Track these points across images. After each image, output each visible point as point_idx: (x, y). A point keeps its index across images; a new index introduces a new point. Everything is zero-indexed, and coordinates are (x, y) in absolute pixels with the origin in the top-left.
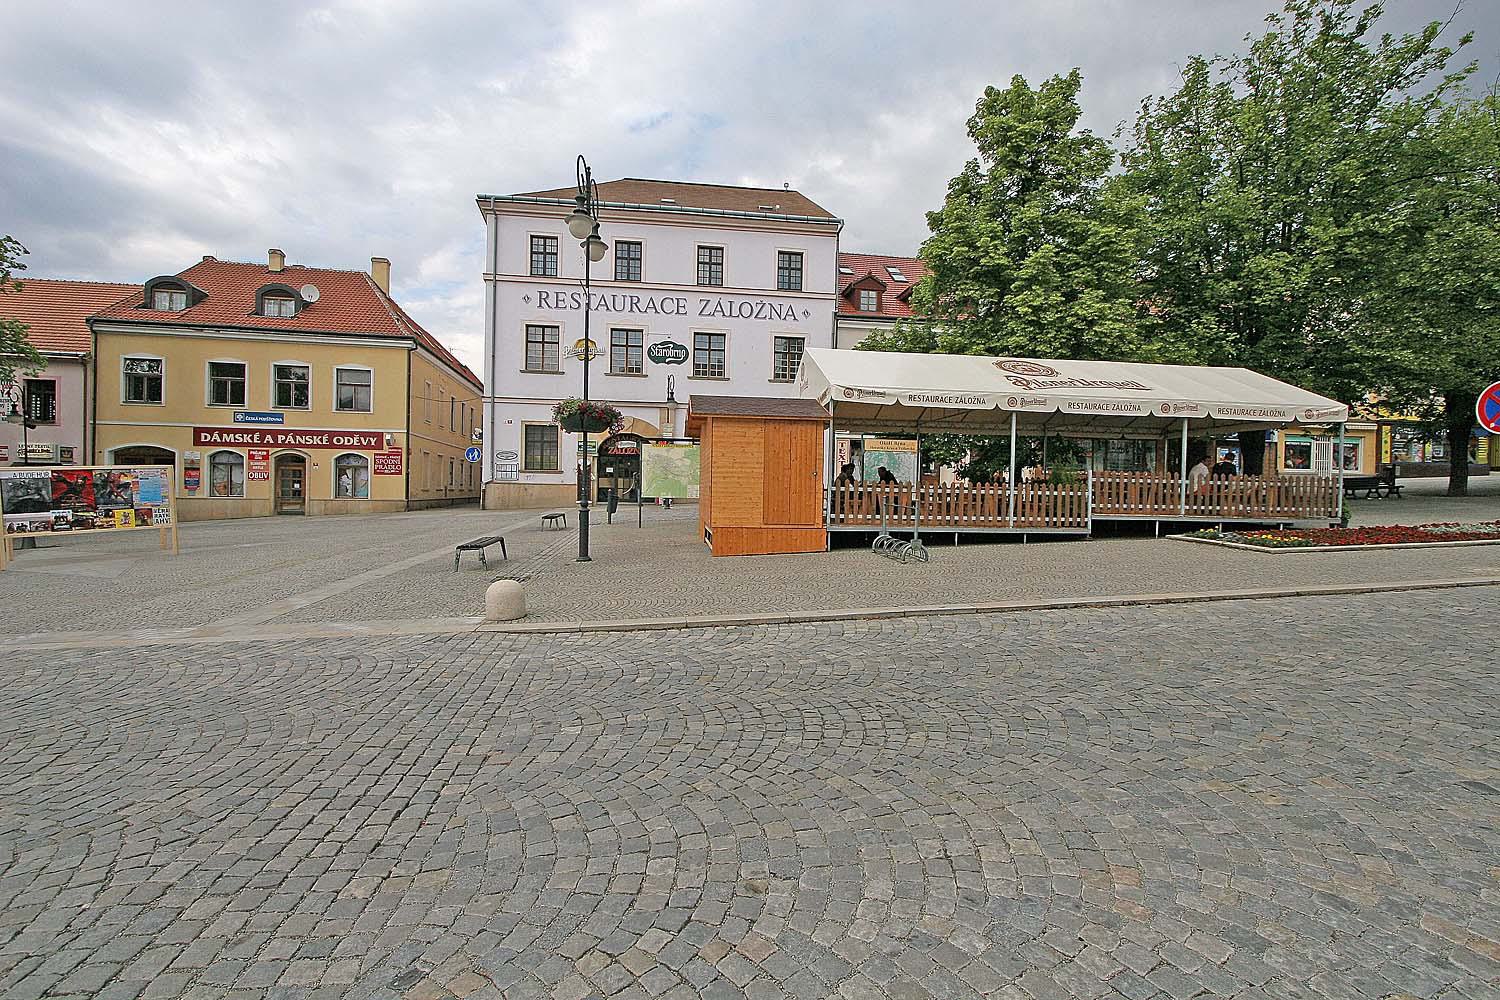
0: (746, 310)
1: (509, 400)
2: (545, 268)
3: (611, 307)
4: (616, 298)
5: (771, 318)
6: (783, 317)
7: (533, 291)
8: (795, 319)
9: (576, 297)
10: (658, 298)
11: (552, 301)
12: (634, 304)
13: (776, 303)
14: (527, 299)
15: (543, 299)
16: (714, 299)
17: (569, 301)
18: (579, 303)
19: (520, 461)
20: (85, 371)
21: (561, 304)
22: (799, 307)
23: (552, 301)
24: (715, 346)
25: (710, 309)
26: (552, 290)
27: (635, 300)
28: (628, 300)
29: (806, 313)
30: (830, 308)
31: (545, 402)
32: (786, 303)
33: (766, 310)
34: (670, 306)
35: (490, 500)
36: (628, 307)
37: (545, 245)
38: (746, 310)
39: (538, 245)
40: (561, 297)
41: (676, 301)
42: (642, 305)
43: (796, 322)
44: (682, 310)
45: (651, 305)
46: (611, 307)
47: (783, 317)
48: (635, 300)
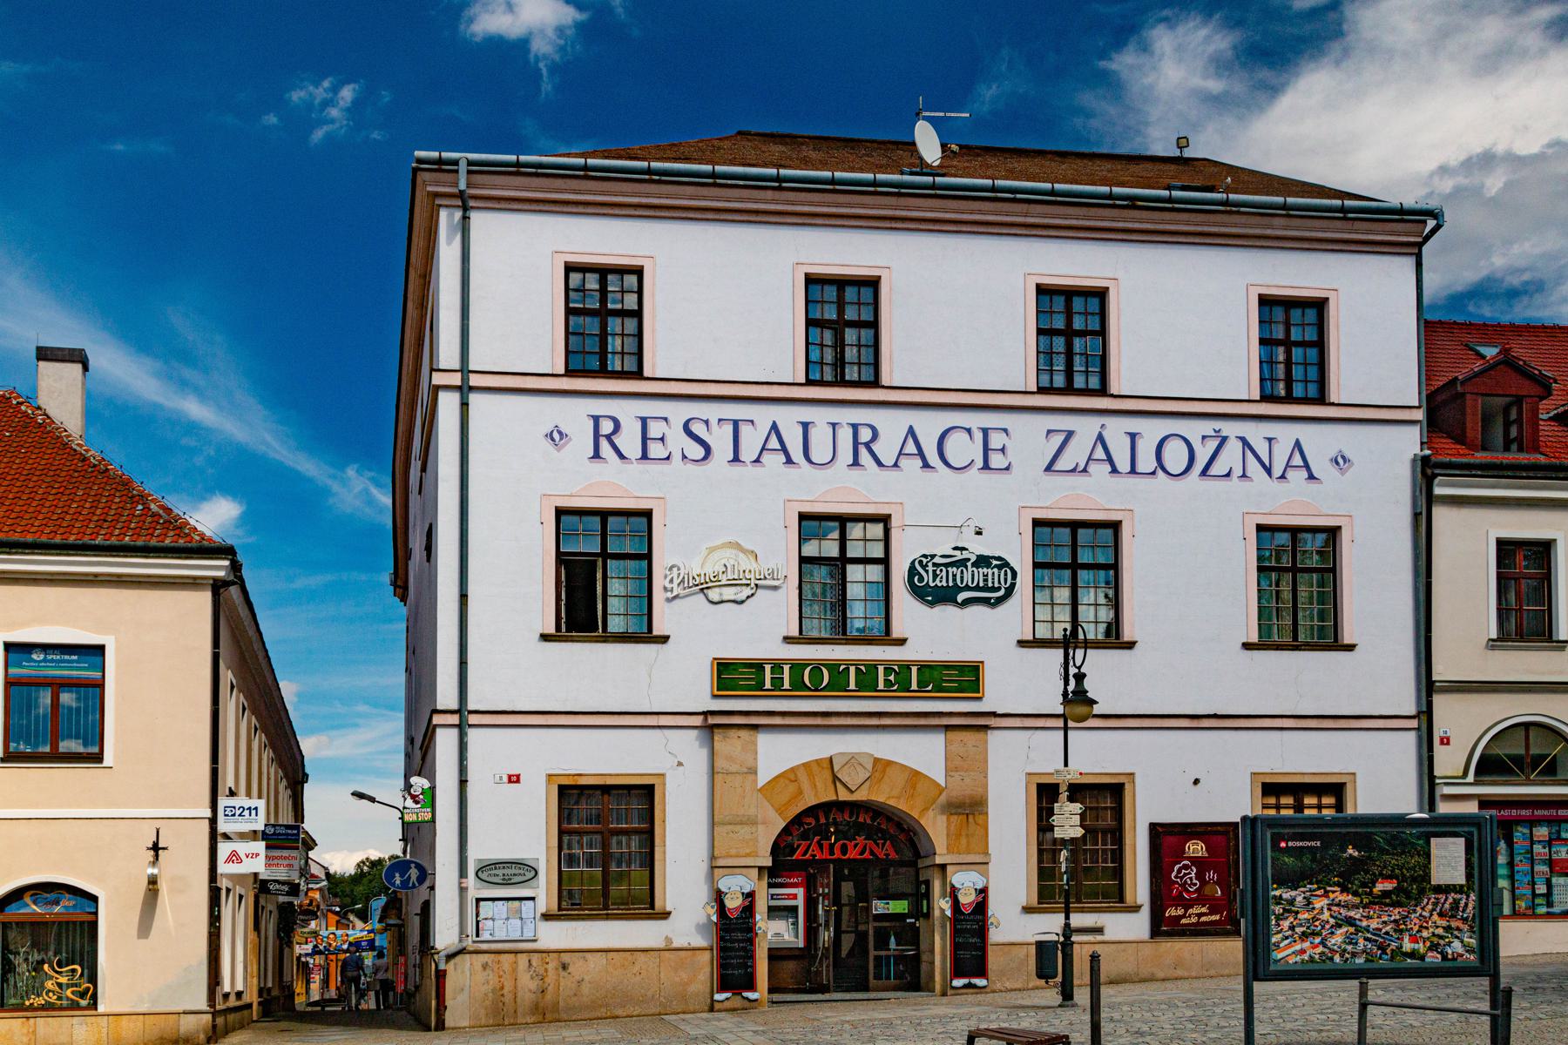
0: (1175, 456)
1: (507, 718)
2: (1289, 381)
3: (796, 453)
4: (813, 432)
5: (1244, 475)
6: (1277, 472)
7: (575, 415)
8: (1311, 477)
9: (698, 429)
10: (929, 426)
11: (629, 440)
12: (863, 446)
13: (1256, 433)
14: (556, 437)
15: (603, 438)
16: (1086, 429)
17: (678, 441)
18: (708, 449)
19: (544, 892)
20: (795, 924)
21: (655, 450)
22: (1321, 442)
23: (629, 440)
24: (1284, 559)
25: (1075, 454)
26: (628, 412)
27: (607, 427)
28: (845, 435)
29: (1340, 461)
30: (1408, 443)
31: (664, 720)
32: (1286, 434)
33: (1231, 456)
34: (963, 449)
35: (458, 1009)
36: (846, 454)
37: (603, 291)
38: (1175, 456)
39: (1086, 314)
40: (655, 430)
41: (979, 436)
42: (886, 449)
43: (1313, 486)
44: (996, 460)
45: (911, 448)
46: (796, 453)
47: (1277, 472)
48: (865, 435)
